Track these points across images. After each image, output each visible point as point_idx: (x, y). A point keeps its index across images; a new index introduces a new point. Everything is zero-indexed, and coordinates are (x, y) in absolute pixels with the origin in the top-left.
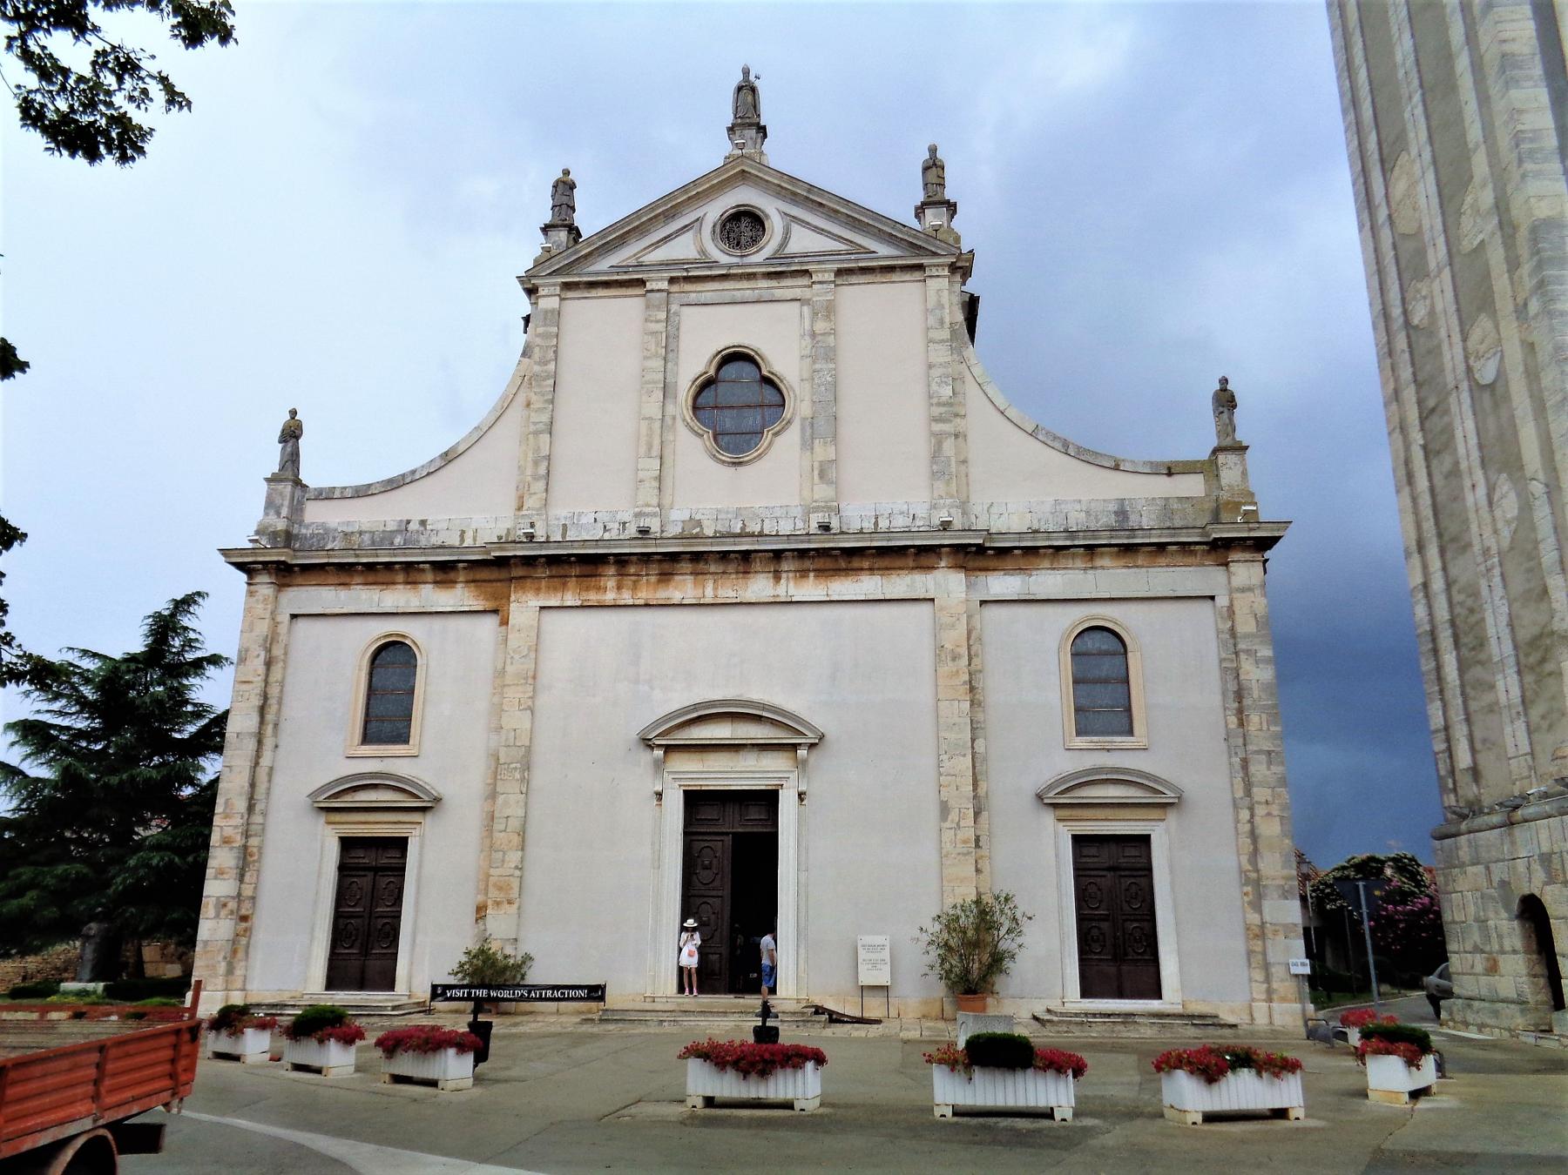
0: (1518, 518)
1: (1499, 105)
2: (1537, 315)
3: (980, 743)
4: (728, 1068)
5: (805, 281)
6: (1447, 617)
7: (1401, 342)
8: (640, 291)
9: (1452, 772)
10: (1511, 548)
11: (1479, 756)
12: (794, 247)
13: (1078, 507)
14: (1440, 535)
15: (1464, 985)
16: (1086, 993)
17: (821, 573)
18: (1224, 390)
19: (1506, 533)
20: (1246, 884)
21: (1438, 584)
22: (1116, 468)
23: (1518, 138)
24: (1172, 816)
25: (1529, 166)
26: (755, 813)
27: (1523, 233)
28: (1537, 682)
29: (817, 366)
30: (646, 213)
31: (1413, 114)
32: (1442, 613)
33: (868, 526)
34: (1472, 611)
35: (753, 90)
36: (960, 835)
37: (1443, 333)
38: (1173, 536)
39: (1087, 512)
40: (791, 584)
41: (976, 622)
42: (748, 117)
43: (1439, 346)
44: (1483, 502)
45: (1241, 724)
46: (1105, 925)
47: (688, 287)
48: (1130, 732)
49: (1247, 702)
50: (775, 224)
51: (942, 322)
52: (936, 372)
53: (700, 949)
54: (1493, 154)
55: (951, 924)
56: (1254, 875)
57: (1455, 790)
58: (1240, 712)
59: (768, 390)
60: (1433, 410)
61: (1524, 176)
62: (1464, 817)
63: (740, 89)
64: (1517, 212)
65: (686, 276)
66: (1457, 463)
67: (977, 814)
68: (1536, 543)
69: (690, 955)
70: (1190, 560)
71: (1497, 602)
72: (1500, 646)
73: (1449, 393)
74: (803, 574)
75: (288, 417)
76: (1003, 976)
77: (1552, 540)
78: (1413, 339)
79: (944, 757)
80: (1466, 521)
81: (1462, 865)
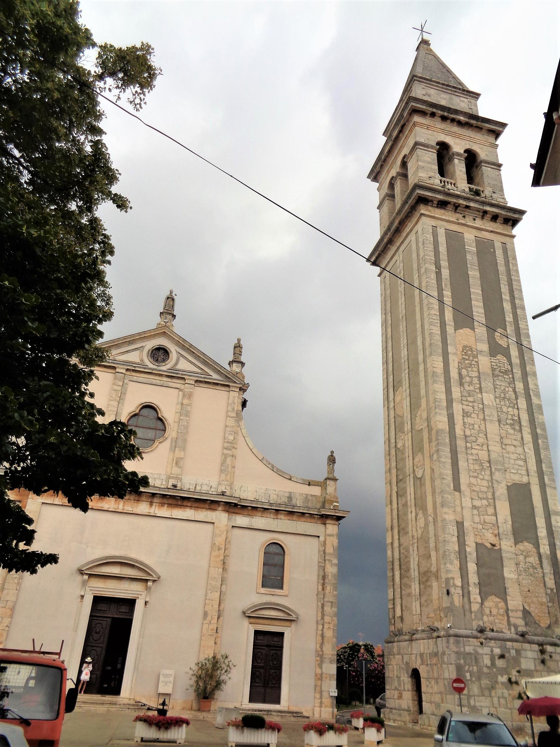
0: (424, 527)
1: (431, 387)
2: (435, 461)
3: (224, 586)
4: (153, 726)
5: (182, 382)
6: (398, 557)
7: (393, 452)
8: (113, 371)
9: (394, 617)
10: (421, 538)
11: (403, 612)
12: (180, 366)
13: (275, 493)
14: (399, 526)
15: (390, 703)
16: (251, 700)
17: (170, 505)
18: (332, 456)
19: (420, 532)
20: (318, 656)
21: (396, 544)
22: (290, 479)
23: (435, 400)
24: (293, 625)
25: (437, 410)
26: (124, 609)
27: (434, 432)
28: (425, 588)
29: (182, 418)
30: (122, 340)
31: (405, 375)
32: (397, 556)
33: (192, 488)
34: (406, 557)
35: (173, 300)
36: (211, 627)
37: (407, 455)
38: (308, 510)
39: (277, 495)
40: (157, 508)
41: (229, 535)
42: (169, 310)
43: (405, 458)
44: (414, 519)
45: (323, 589)
46: (262, 671)
47: (133, 374)
48: (281, 588)
49: (327, 581)
50: (174, 355)
51: (233, 409)
52: (228, 429)
53: (91, 672)
54: (427, 401)
55: (202, 667)
56: (321, 653)
57: (394, 624)
58: (323, 584)
59: (159, 423)
60: (401, 480)
61: (436, 413)
62: (396, 635)
63: (168, 298)
64: (432, 423)
65: (133, 369)
66: (407, 502)
67: (218, 618)
68: (429, 538)
69: (86, 674)
70: (312, 520)
71: (415, 556)
72: (414, 573)
73: (406, 476)
74: (162, 504)
76: (222, 692)
77: (433, 539)
78: (397, 452)
79: (209, 592)
80: (408, 523)
81: (394, 655)
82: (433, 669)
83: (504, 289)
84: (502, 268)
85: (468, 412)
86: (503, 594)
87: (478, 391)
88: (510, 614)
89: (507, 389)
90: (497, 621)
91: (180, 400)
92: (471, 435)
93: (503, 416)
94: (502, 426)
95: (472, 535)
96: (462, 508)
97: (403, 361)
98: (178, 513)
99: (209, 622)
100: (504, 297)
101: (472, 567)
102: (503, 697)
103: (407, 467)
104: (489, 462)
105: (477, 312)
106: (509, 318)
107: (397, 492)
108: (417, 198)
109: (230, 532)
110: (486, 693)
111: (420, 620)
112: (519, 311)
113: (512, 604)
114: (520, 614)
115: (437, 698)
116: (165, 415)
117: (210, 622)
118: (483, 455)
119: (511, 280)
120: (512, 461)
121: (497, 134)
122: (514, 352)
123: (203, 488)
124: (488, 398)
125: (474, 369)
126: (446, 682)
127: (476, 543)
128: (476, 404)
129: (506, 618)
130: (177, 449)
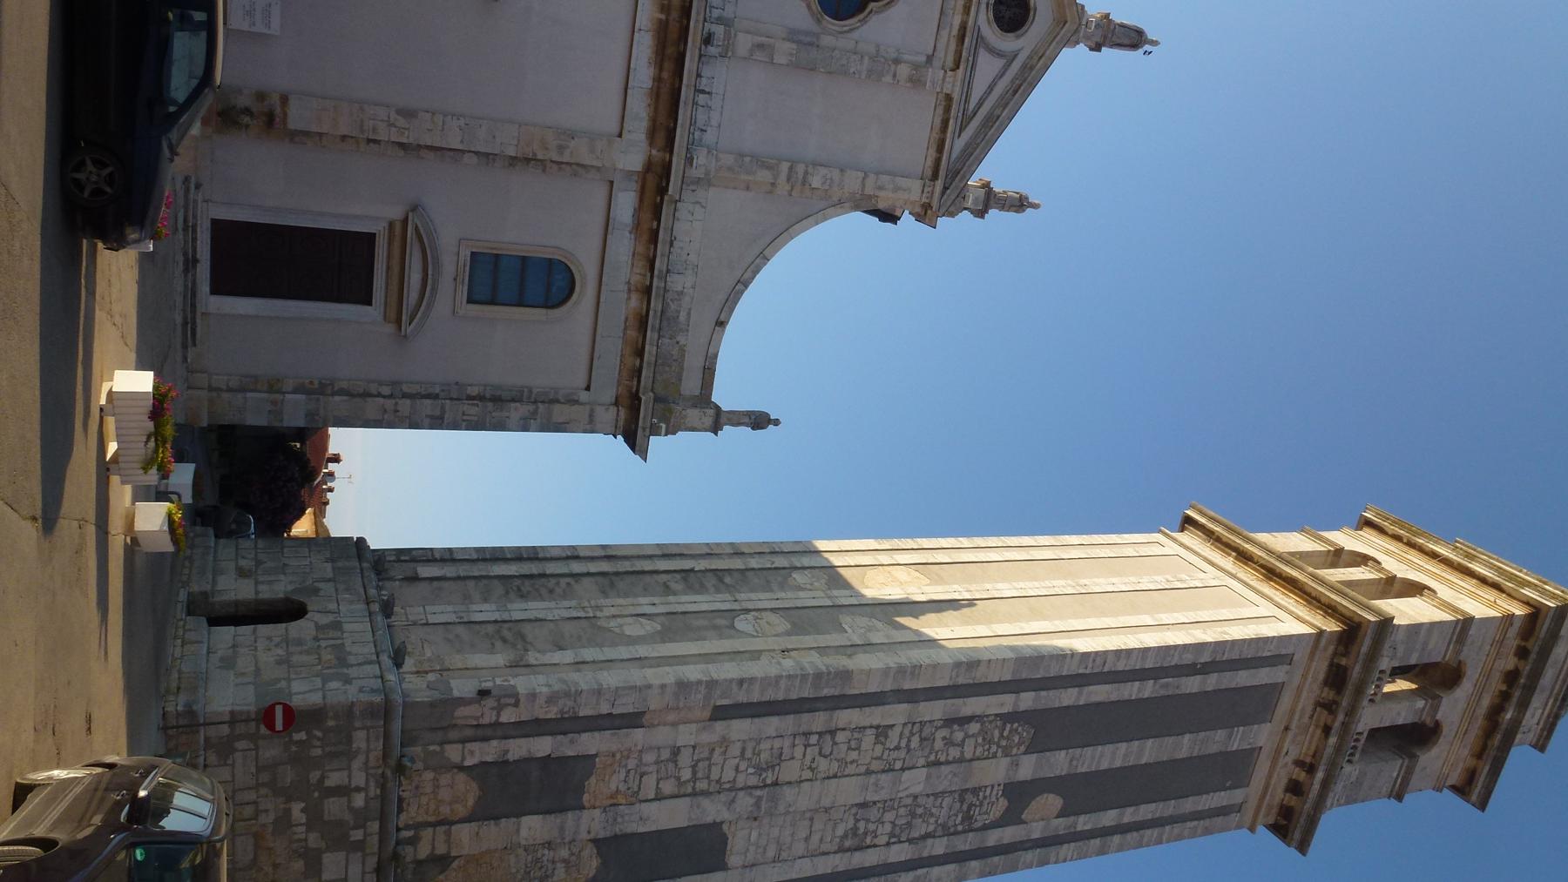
3: (475, 159)
12: (984, 58)
14: (617, 574)
34: (551, 591)
45: (470, 398)
50: (1008, 43)
51: (881, 188)
52: (836, 174)
58: (481, 398)
67: (401, 145)
68: (601, 646)
71: (556, 612)
72: (519, 610)
79: (462, 122)
80: (626, 596)
82: (308, 652)
83: (1146, 811)
84: (1189, 805)
85: (886, 737)
86: (483, 813)
87: (932, 758)
88: (441, 829)
89: (932, 820)
90: (424, 800)
91: (906, 57)
92: (835, 743)
93: (873, 813)
94: (854, 810)
95: (614, 748)
96: (674, 724)
97: (988, 586)
98: (645, 46)
100: (1130, 810)
101: (543, 746)
102: (257, 813)
103: (753, 596)
104: (776, 784)
105: (1102, 756)
106: (1084, 823)
107: (692, 570)
108: (1356, 619)
110: (265, 777)
111: (415, 624)
112: (1097, 842)
113: (464, 832)
114: (441, 850)
115: (244, 662)
117: (393, 125)
118: (790, 771)
119: (1163, 825)
120: (775, 832)
121: (1462, 790)
122: (1009, 834)
124: (915, 781)
125: (979, 749)
126: (283, 684)
127: (596, 755)
128: (902, 754)
129: (431, 819)
130: (794, 46)
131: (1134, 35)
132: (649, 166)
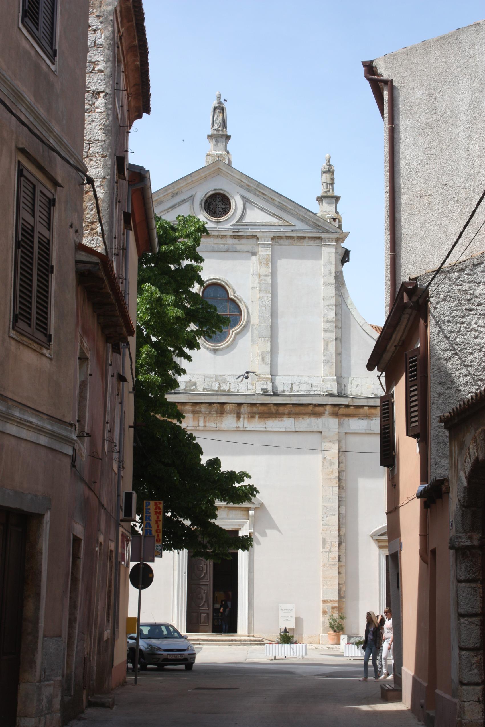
3: (343, 508)
40: (246, 421)
50: (237, 202)
63: (215, 109)
67: (340, 544)
74: (252, 416)
75: (124, 465)
98: (273, 424)
99: (328, 550)
109: (344, 441)
116: (239, 294)
117: (330, 550)
123: (301, 389)
131: (217, 111)
132: (335, 415)
